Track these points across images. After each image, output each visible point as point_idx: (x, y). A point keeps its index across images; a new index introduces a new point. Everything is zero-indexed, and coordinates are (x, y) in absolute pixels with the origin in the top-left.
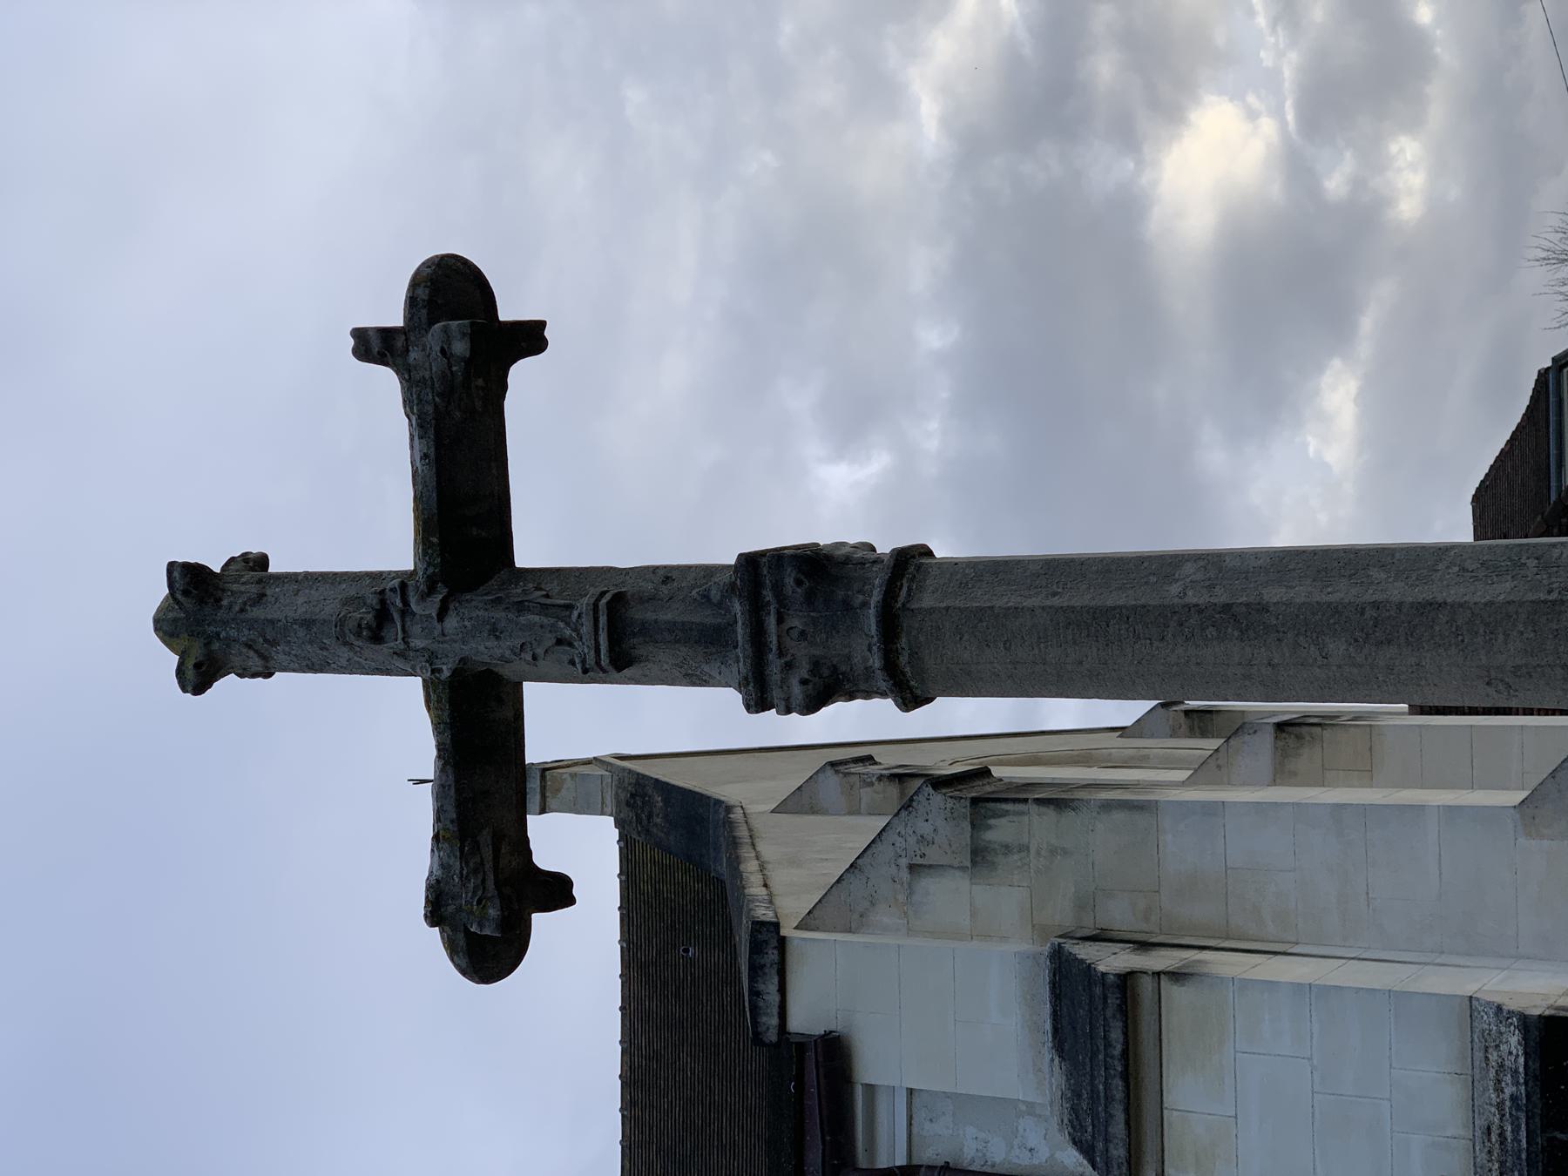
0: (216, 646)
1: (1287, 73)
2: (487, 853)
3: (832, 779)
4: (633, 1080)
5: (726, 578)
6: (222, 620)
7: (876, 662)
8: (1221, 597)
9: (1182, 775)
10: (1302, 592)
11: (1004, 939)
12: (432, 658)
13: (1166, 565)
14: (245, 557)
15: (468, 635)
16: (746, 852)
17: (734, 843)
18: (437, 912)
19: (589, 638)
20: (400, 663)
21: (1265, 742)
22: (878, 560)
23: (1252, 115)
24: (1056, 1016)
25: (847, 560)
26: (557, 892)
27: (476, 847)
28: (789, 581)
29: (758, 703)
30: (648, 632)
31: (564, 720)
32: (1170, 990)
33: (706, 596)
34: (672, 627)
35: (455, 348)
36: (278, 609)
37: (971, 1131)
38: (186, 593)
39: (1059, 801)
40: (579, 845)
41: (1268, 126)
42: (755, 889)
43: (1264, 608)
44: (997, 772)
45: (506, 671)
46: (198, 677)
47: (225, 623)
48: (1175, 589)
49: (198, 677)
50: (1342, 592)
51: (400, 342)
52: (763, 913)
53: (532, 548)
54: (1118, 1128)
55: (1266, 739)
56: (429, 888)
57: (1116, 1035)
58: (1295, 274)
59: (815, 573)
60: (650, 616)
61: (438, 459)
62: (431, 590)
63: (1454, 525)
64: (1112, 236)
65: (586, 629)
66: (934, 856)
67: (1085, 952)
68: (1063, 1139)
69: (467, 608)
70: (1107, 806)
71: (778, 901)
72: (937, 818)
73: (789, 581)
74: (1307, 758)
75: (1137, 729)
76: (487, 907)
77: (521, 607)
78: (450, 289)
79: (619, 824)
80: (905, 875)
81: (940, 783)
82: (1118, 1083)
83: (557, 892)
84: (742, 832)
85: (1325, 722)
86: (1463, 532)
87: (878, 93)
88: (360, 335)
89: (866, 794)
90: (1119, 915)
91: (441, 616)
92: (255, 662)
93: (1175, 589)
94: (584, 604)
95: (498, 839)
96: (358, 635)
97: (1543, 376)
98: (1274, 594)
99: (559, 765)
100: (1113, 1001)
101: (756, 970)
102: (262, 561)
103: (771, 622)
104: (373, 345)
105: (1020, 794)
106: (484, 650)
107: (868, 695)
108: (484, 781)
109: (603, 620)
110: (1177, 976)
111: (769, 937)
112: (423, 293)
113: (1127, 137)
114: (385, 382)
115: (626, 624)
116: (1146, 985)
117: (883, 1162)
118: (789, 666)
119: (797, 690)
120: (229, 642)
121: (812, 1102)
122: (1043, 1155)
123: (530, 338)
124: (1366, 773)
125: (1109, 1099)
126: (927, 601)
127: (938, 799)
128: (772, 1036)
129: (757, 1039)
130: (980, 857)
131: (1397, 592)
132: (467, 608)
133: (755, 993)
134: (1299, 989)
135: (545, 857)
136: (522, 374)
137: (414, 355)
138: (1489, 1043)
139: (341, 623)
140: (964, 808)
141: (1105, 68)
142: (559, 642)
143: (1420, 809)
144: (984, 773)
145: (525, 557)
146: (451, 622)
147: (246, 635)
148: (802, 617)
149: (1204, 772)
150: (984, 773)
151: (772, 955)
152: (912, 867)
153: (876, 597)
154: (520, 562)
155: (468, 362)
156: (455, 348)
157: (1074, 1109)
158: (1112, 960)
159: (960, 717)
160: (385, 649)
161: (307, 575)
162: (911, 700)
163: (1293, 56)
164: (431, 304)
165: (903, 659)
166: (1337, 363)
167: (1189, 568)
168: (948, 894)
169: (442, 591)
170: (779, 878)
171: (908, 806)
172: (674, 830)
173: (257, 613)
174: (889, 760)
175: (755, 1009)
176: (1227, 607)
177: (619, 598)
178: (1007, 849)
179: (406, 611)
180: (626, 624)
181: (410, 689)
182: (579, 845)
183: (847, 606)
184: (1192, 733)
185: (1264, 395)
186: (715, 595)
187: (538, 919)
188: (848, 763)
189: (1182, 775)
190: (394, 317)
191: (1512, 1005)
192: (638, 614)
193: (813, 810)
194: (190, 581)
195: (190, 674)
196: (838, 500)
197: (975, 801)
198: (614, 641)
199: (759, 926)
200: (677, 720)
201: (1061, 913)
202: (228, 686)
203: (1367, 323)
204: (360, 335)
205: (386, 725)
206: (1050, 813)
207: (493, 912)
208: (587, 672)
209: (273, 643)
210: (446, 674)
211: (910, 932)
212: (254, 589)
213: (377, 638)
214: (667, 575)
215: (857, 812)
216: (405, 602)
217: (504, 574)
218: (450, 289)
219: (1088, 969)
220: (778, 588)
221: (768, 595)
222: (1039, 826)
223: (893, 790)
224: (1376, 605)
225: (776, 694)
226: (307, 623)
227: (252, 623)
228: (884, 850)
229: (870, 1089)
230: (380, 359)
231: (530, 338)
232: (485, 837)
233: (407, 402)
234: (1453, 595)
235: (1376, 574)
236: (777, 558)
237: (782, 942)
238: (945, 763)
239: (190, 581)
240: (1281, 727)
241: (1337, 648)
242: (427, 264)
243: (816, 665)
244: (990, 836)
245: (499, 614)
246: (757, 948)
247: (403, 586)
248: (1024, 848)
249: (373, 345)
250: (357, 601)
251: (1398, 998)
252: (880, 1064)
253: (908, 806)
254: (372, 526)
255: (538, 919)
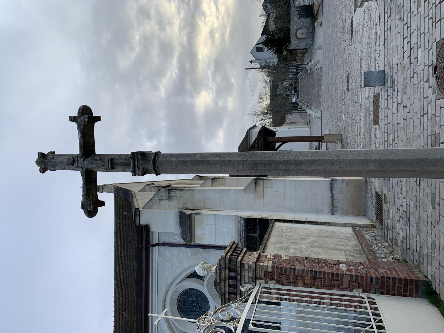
0: (46, 166)
1: (214, 88)
2: (91, 198)
3: (148, 187)
4: (116, 233)
5: (129, 156)
6: (47, 162)
7: (152, 168)
8: (202, 159)
9: (199, 186)
10: (213, 159)
11: (173, 209)
12: (82, 168)
13: (195, 155)
14: (51, 152)
15: (88, 164)
16: (134, 198)
17: (132, 196)
18: (83, 207)
19: (108, 165)
20: (76, 168)
21: (210, 181)
22: (153, 154)
23: (209, 94)
24: (180, 220)
25: (148, 153)
26: (102, 204)
27: (89, 197)
28: (139, 156)
29: (134, 174)
30: (117, 164)
31: (104, 178)
32: (196, 216)
33: (126, 159)
34: (121, 163)
35: (86, 120)
36: (57, 160)
37: (167, 237)
38: (41, 157)
39: (181, 189)
40: (108, 198)
41: (211, 95)
42: (135, 203)
43: (208, 161)
44: (172, 185)
45: (94, 170)
46: (43, 171)
47: (48, 162)
48: (196, 158)
49: (43, 171)
50: (219, 159)
51: (77, 119)
52: (136, 207)
53: (98, 151)
54: (189, 236)
55: (211, 180)
56: (81, 203)
57: (189, 223)
58: (215, 117)
59: (143, 156)
60: (117, 161)
61: (83, 137)
62: (82, 157)
63: (236, 150)
64: (190, 110)
65: (107, 163)
66: (163, 198)
67: (182, 210)
68: (181, 238)
69: (88, 161)
70: (188, 190)
71: (139, 205)
72: (163, 192)
73: (139, 156)
74: (216, 183)
75: (193, 179)
76: (91, 206)
77: (96, 160)
78: (85, 111)
79: (114, 194)
80: (158, 201)
81: (164, 187)
82: (189, 230)
83: (102, 204)
84: (134, 195)
85: (218, 178)
86: (237, 150)
87: (155, 88)
88: (70, 117)
89: (153, 189)
90: (189, 206)
91: (83, 161)
92: (53, 169)
93: (196, 158)
94: (107, 160)
95: (93, 196)
96: (70, 164)
97: (248, 131)
98: (209, 159)
99: (105, 185)
100: (188, 218)
101: (135, 215)
102: (54, 153)
103: (136, 163)
104: (72, 119)
105: (175, 189)
106: (90, 167)
107: (151, 173)
108: (91, 187)
109: (110, 162)
110: (197, 214)
111: (138, 211)
112: (81, 111)
113: (192, 96)
114: (74, 125)
115: (113, 163)
116: (193, 215)
117: (99, 194)
118: (139, 169)
119: (140, 173)
120: (48, 165)
121: (144, 235)
122: (178, 240)
123: (98, 119)
124: (224, 185)
125: (187, 232)
126: (160, 160)
127: (163, 189)
128: (138, 225)
129: (136, 226)
130: (169, 198)
131: (226, 159)
132: (88, 161)
133: (135, 219)
134: (214, 215)
135: (100, 199)
136: (97, 124)
137: (79, 121)
138: (239, 222)
139: (67, 162)
140: (167, 191)
141: (188, 86)
142: (103, 165)
143: (230, 190)
144: (170, 185)
145: (97, 152)
146: (85, 162)
147: (51, 164)
148: (140, 162)
149: (202, 185)
150: (170, 185)
151: (138, 213)
152: (159, 199)
153: (152, 159)
154: (96, 153)
155: (88, 122)
156: (86, 120)
157: (182, 234)
158: (188, 212)
159: (166, 178)
160: (74, 166)
161: (61, 155)
162: (158, 174)
163: (215, 85)
164: (82, 113)
165: (156, 168)
166: (221, 129)
167: (198, 155)
168: (165, 203)
169: (84, 157)
170: (139, 202)
171: (159, 190)
172: (123, 196)
173: (53, 161)
174: (156, 184)
175: (135, 221)
176: (203, 161)
177: (112, 159)
178: (173, 196)
179: (78, 160)
180: (113, 163)
181: (79, 172)
182: (108, 198)
183: (148, 160)
184: (200, 180)
185: (211, 134)
186: (128, 158)
187: (99, 208)
188: (150, 184)
189: (199, 186)
190: (76, 115)
191: (242, 216)
192: (115, 161)
193: (145, 191)
194: (42, 156)
195: (42, 170)
196: (149, 146)
197: (169, 190)
198: (112, 165)
199: (136, 209)
200: (123, 178)
201: (181, 206)
202: (48, 172)
203: (225, 124)
204: (70, 117)
205: (74, 179)
206: (180, 191)
207: (92, 207)
208: (107, 170)
209: (56, 165)
210: (84, 170)
211: (159, 209)
212: (52, 157)
213: (73, 165)
214: (120, 155)
215: (151, 192)
216: (78, 159)
217: (94, 155)
218: (85, 111)
219: (185, 213)
220: (137, 157)
221: (136, 158)
222: (178, 193)
223: (157, 188)
224: (223, 161)
225: (137, 173)
226: (61, 162)
227: (52, 162)
228: (155, 197)
229: (153, 232)
230: (74, 121)
231: (98, 119)
232: (91, 196)
233: (78, 128)
234: (233, 159)
235: (223, 156)
236: (137, 153)
237: (139, 211)
238: (164, 184)
239: (42, 156)
240: (212, 179)
241: (218, 167)
242: (81, 107)
243: (143, 169)
244: (171, 195)
245: (93, 161)
246: (135, 212)
247: (77, 157)
248: (176, 196)
249: (72, 119)
250: (70, 159)
251: (227, 216)
252: (153, 229)
253: (159, 190)
254: (73, 148)
255: (99, 208)
